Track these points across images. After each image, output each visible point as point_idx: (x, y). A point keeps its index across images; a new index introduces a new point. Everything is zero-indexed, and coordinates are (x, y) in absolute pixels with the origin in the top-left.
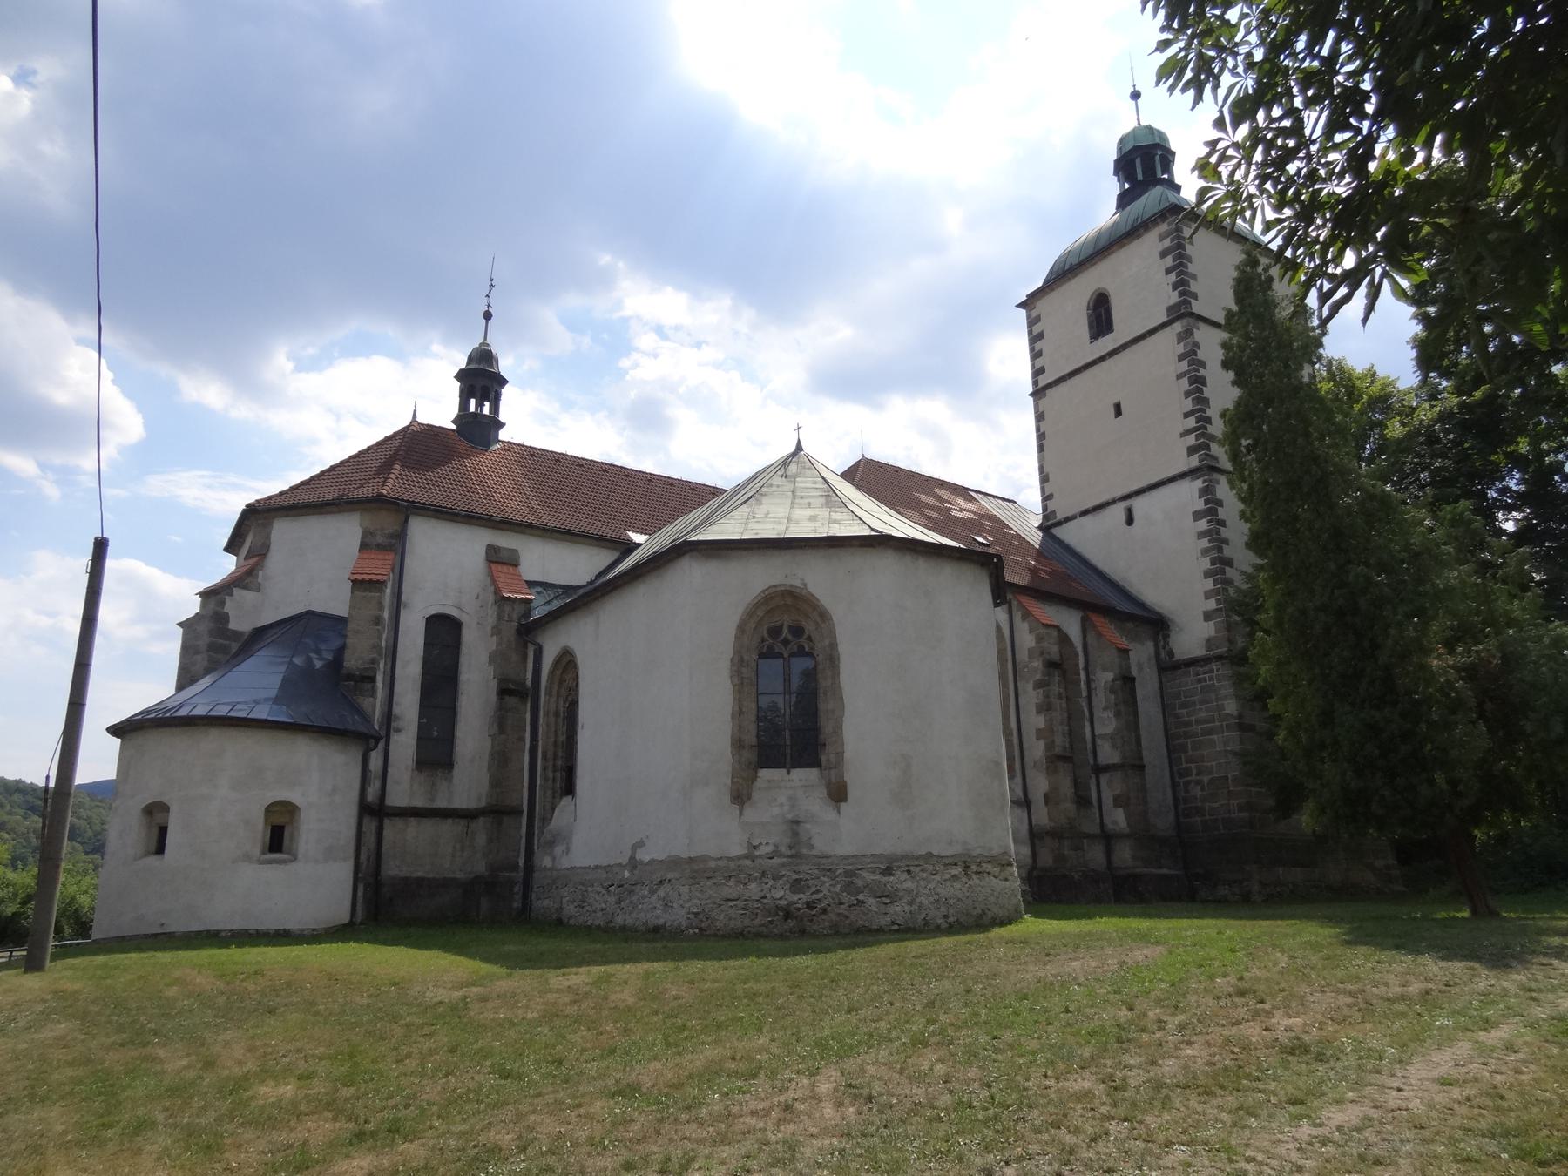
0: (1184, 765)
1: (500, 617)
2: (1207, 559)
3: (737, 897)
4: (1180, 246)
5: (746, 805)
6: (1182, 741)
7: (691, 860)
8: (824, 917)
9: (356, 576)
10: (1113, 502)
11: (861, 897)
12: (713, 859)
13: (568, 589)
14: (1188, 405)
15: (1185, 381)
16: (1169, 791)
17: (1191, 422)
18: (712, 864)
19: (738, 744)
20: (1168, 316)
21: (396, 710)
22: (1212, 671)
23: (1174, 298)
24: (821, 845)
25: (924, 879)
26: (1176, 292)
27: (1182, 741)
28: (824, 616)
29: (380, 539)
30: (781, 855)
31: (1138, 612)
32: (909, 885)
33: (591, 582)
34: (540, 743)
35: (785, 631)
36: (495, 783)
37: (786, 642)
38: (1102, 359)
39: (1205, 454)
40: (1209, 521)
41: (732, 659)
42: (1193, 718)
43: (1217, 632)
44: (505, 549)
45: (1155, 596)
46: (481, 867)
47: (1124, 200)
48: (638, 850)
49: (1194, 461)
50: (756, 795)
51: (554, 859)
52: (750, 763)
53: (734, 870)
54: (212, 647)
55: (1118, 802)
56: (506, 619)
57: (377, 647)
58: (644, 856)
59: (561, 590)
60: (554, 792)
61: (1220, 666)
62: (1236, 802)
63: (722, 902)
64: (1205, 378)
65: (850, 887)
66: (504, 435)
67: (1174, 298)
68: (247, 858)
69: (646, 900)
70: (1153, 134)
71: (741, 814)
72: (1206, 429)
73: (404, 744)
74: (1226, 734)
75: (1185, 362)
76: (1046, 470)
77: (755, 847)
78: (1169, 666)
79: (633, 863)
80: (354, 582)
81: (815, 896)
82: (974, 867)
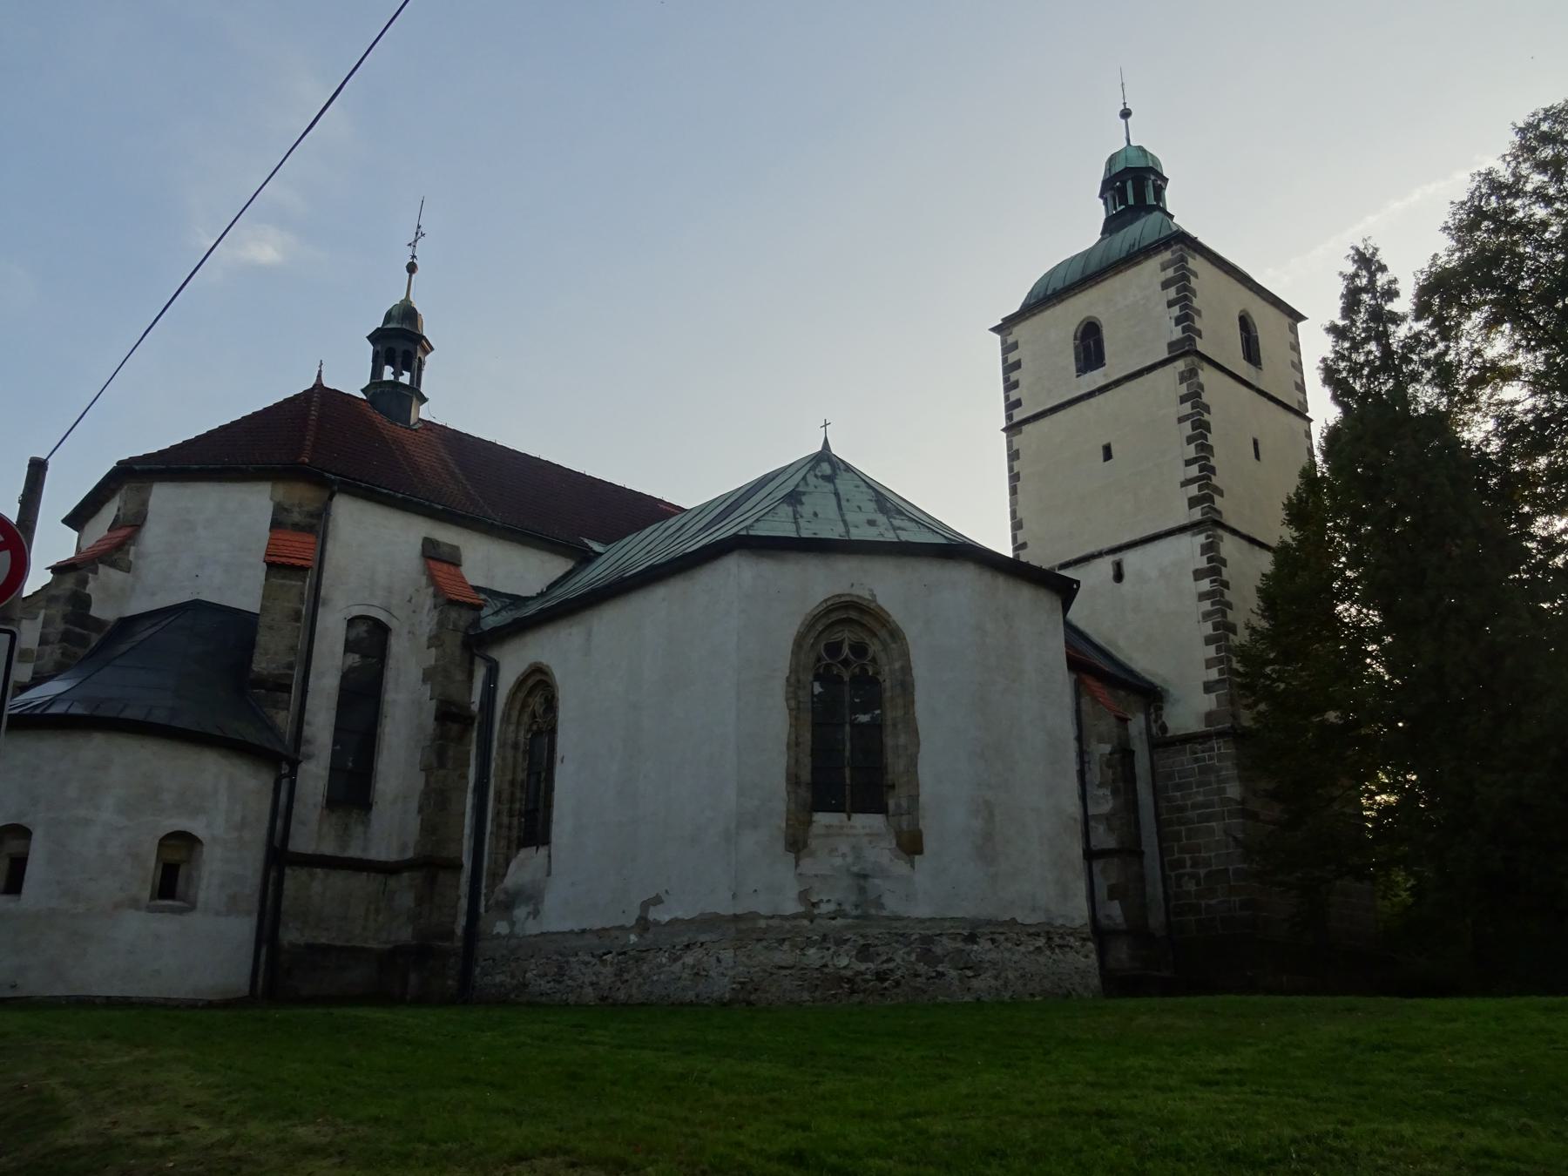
0: (1177, 856)
1: (441, 624)
2: (1209, 624)
4: (1185, 278)
9: (273, 559)
10: (1100, 554)
11: (940, 968)
13: (516, 601)
14: (1191, 451)
15: (1188, 424)
18: (762, 923)
19: (793, 779)
20: (1169, 353)
21: (307, 731)
22: (1212, 749)
23: (1177, 333)
24: (893, 905)
26: (1180, 328)
27: (1177, 828)
28: (896, 634)
29: (296, 517)
30: (845, 916)
31: (1123, 676)
32: (993, 955)
35: (846, 651)
36: (429, 829)
37: (846, 663)
38: (1090, 395)
40: (1212, 582)
41: (788, 679)
42: (1189, 803)
45: (1143, 662)
46: (405, 934)
47: (1112, 225)
48: (652, 908)
49: (1197, 514)
50: (814, 843)
51: (512, 924)
53: (789, 931)
54: (66, 637)
55: (1113, 893)
56: (451, 627)
57: (293, 649)
58: (660, 915)
59: (507, 600)
61: (1221, 744)
63: (775, 971)
64: (1209, 424)
65: (927, 956)
66: (425, 412)
67: (1177, 333)
68: (134, 904)
70: (1146, 157)
71: (797, 865)
72: (1210, 479)
73: (314, 775)
75: (1188, 404)
76: (1019, 515)
77: (814, 905)
78: (1162, 742)
79: (643, 924)
80: (271, 566)
81: (885, 966)
82: (1057, 940)
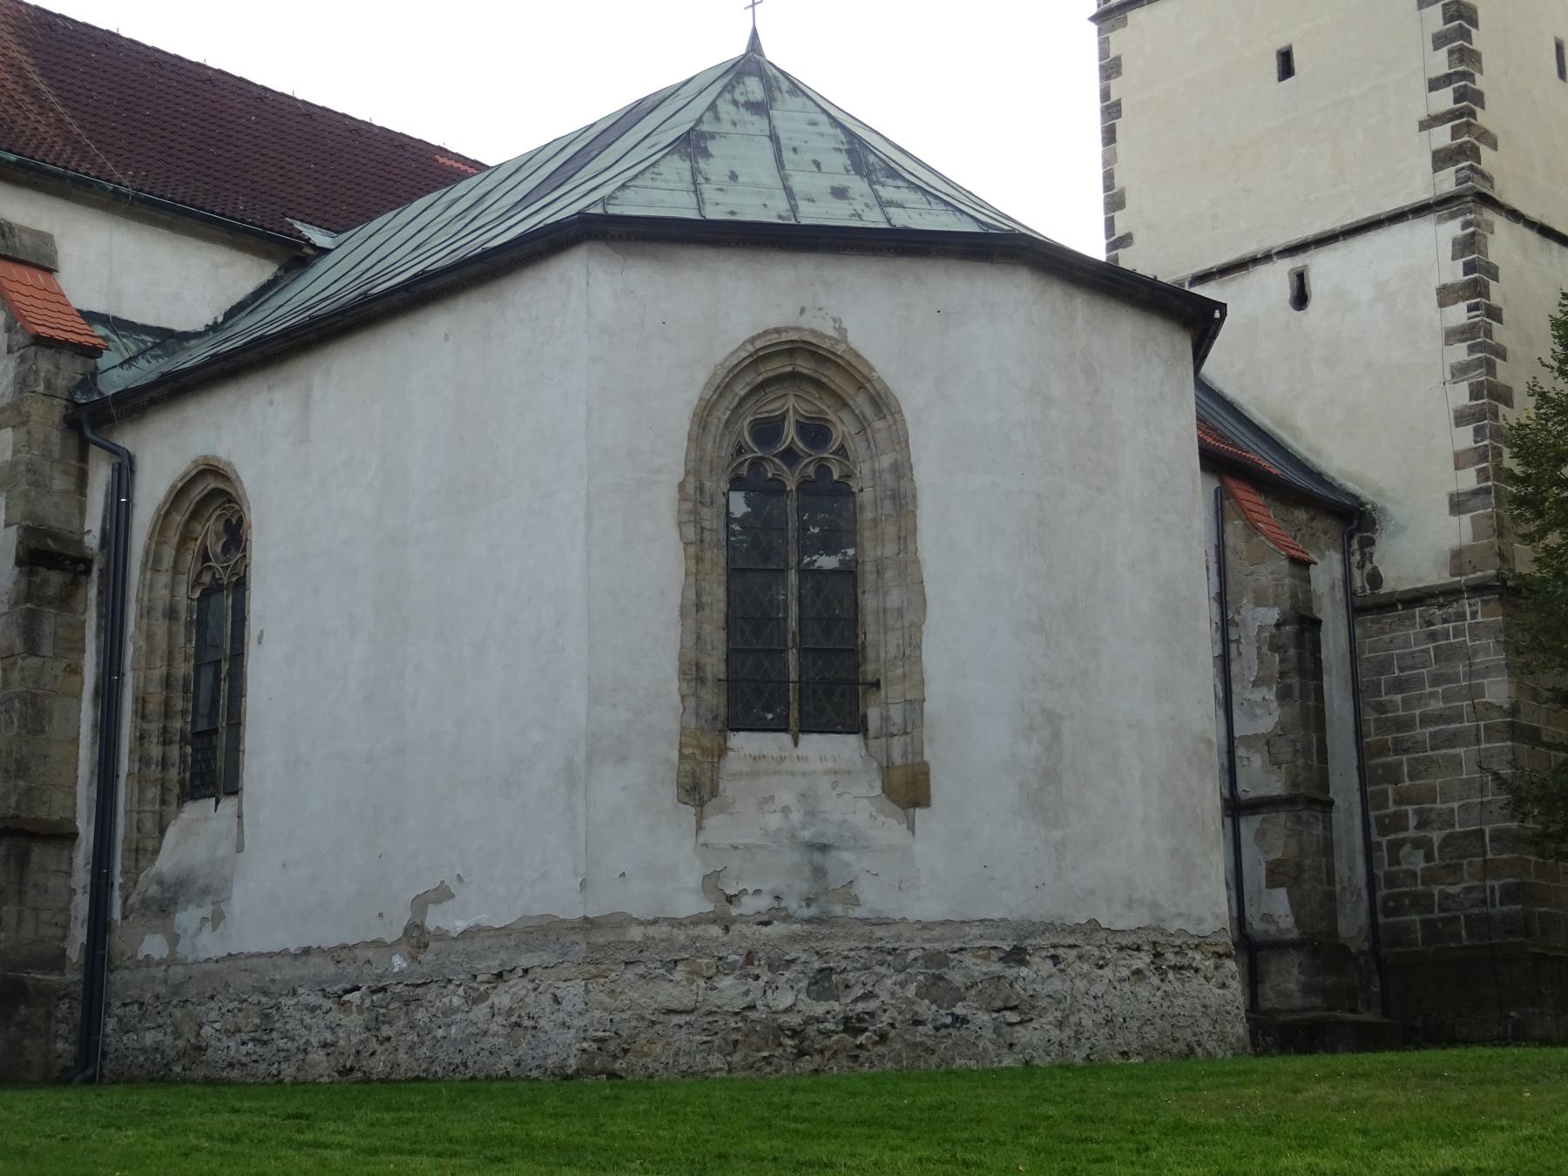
3: (691, 1005)
5: (708, 808)
6: (1391, 758)
7: (588, 924)
8: (880, 1049)
10: (1267, 257)
11: (959, 1010)
12: (640, 923)
13: (168, 339)
14: (1440, 63)
16: (1360, 860)
17: (1444, 100)
18: (636, 933)
19: (693, 673)
22: (1461, 616)
24: (875, 898)
25: (1082, 975)
27: (1391, 758)
28: (882, 403)
30: (788, 918)
32: (1056, 985)
33: (214, 328)
34: (129, 679)
35: (790, 433)
37: (790, 456)
39: (1471, 168)
40: (1470, 309)
41: (682, 486)
43: (1476, 536)
44: (23, 229)
49: (1447, 182)
50: (727, 788)
51: (174, 940)
52: (715, 718)
53: (684, 947)
55: (1276, 875)
56: (41, 388)
58: (449, 919)
60: (165, 789)
61: (1479, 607)
62: (1497, 884)
65: (936, 987)
69: (458, 1017)
71: (699, 827)
74: (1483, 746)
76: (1119, 183)
77: (730, 899)
79: (417, 937)
81: (860, 1007)
82: (1171, 958)
